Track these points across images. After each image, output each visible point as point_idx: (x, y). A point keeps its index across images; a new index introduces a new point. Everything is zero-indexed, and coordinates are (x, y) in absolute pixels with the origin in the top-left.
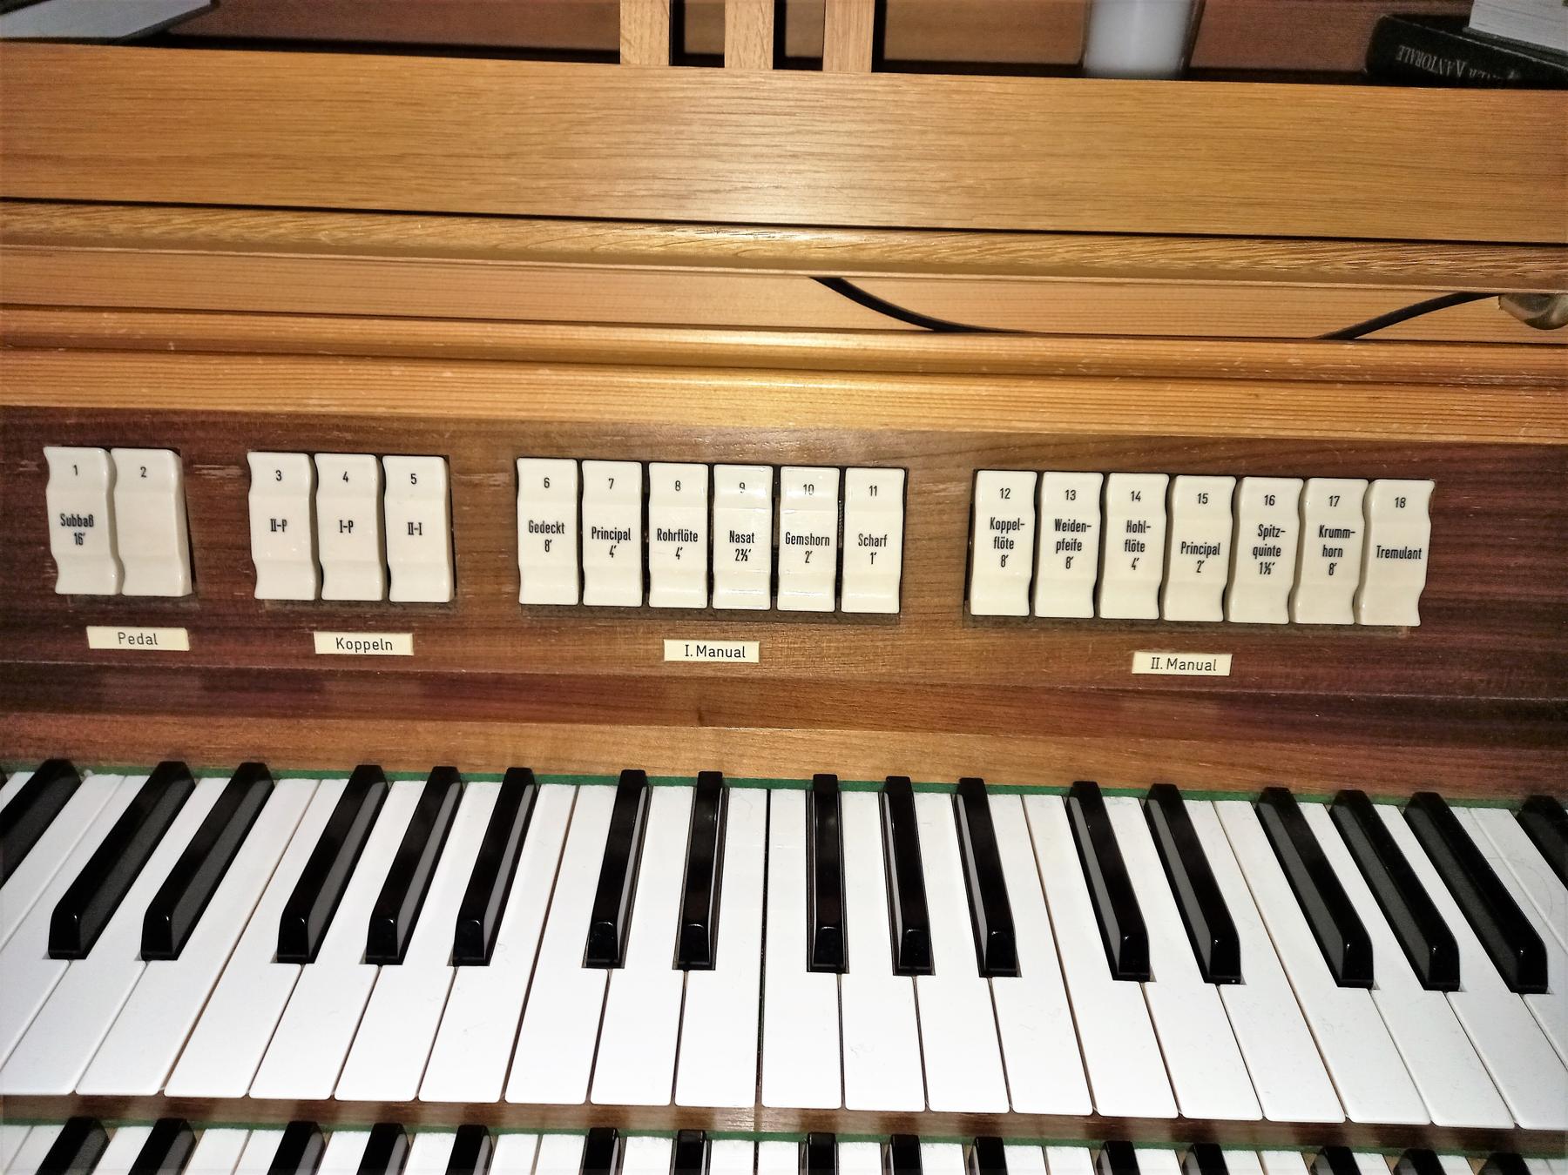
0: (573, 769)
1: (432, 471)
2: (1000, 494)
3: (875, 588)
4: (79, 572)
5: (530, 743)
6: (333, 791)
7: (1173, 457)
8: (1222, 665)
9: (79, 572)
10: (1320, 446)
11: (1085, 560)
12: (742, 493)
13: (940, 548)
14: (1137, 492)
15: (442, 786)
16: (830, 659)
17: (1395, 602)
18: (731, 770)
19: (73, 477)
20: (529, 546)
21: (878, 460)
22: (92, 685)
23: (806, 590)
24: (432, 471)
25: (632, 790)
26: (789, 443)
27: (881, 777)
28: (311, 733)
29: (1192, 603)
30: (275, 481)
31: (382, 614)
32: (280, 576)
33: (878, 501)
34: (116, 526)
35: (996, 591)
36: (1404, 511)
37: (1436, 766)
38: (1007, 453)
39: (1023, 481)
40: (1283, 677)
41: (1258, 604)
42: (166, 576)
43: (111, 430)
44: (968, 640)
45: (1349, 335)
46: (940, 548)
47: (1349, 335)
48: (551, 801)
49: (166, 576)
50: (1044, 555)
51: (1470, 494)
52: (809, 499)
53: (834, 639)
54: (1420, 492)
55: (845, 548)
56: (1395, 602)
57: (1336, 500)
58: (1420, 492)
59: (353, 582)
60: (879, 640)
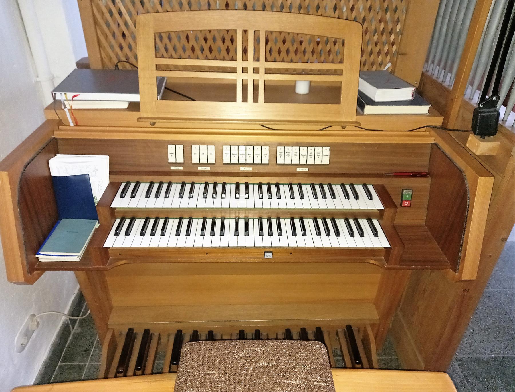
0: (230, 182)
1: (181, 147)
2: (280, 149)
3: (265, 161)
4: (171, 159)
5: (137, 178)
6: (148, 185)
7: (300, 145)
8: (307, 170)
9: (171, 159)
10: (317, 143)
11: (290, 157)
12: (234, 149)
13: (273, 156)
14: (296, 149)
15: (161, 184)
16: (261, 170)
17: (326, 161)
18: (249, 182)
19: (171, 148)
20: (169, 156)
21: (266, 145)
22: (171, 173)
23: (257, 161)
24: (181, 147)
25: (183, 184)
26: (255, 143)
27: (319, 183)
28: (145, 177)
29: (303, 162)
30: (195, 149)
31: (207, 164)
32: (195, 160)
33: (266, 150)
34: (175, 154)
35: (280, 161)
36: (327, 150)
37: (352, 180)
38: (280, 145)
39: (290, 148)
40: (314, 170)
41: (310, 162)
42: (180, 160)
43: (175, 143)
44: (277, 167)
45: (321, 130)
46: (273, 156)
47: (321, 130)
48: (174, 186)
49: (180, 160)
50: (288, 156)
51: (335, 149)
52: (258, 149)
53: (261, 167)
54: (328, 148)
55: (261, 156)
56: (326, 161)
57: (319, 149)
58: (328, 148)
59: (204, 160)
60: (266, 167)
